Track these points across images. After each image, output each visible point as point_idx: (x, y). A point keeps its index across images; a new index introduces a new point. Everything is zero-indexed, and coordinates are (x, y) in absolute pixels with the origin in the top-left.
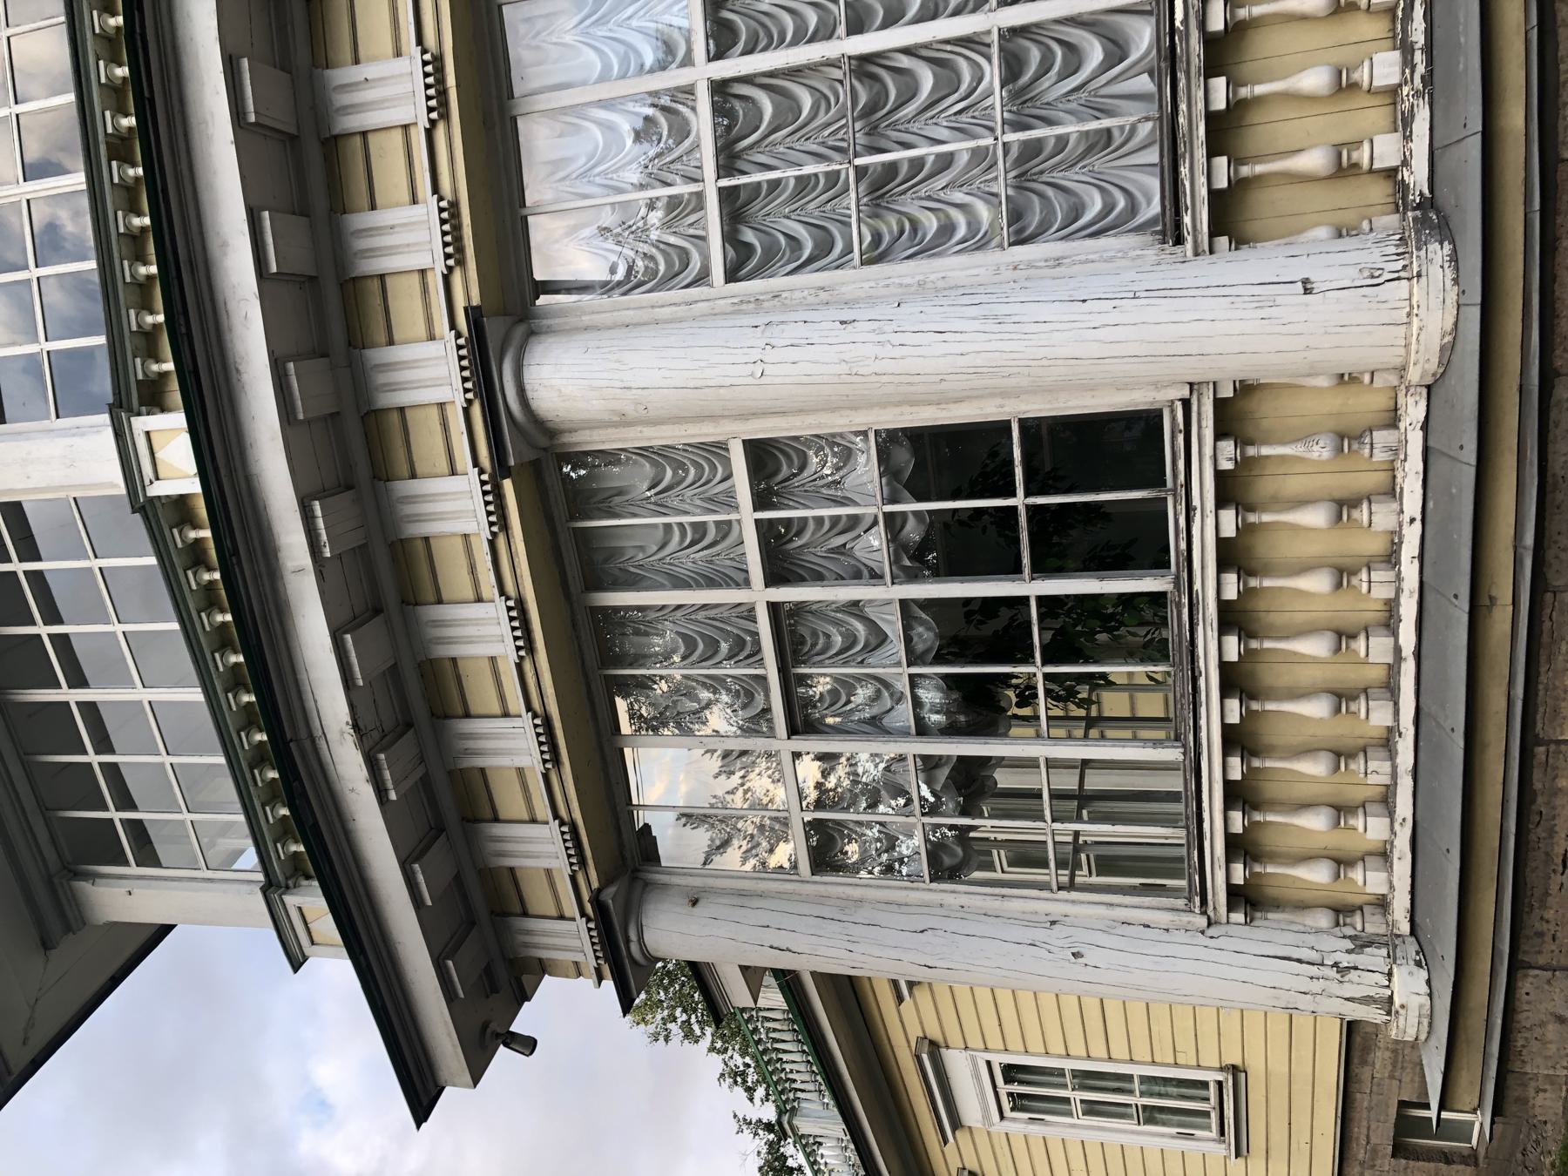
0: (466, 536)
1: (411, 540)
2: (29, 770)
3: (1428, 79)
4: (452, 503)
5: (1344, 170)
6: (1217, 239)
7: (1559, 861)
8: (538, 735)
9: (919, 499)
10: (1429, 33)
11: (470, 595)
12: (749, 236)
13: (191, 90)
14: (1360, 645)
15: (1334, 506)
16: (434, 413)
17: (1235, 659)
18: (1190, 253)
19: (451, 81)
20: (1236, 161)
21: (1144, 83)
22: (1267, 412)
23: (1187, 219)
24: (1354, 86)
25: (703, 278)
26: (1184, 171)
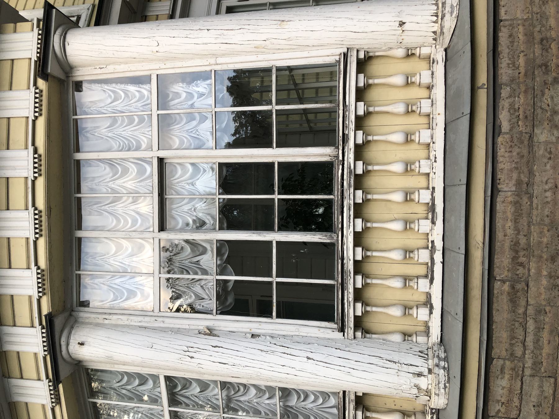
6: (357, 132)
8: (50, 390)
14: (414, 311)
15: (403, 309)
17: (360, 314)
20: (365, 220)
21: (335, 411)
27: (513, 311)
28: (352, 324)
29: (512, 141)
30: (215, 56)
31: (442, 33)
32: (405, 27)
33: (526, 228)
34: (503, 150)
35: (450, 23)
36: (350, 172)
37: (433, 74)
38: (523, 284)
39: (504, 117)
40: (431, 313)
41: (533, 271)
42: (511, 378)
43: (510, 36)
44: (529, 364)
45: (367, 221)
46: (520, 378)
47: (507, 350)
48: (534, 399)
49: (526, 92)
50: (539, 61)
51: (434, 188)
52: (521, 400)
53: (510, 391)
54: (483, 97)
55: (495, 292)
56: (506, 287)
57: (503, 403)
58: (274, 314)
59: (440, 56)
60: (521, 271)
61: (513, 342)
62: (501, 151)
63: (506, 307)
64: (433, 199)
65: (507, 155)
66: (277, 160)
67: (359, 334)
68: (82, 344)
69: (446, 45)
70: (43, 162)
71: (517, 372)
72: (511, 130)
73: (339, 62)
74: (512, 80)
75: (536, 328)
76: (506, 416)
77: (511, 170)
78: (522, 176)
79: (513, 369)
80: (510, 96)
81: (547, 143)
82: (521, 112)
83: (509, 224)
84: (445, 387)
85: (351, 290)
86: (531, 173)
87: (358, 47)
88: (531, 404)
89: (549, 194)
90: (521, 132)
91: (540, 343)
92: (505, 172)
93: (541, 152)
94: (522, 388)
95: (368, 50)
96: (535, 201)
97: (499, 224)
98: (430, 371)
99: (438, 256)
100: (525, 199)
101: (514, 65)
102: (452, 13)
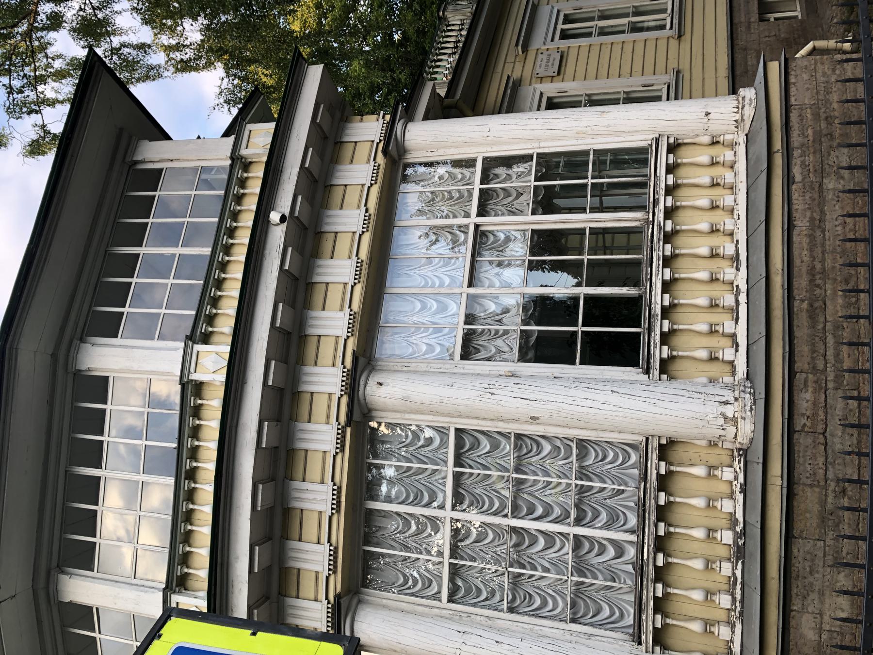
0: (317, 572)
1: (294, 509)
2: (65, 635)
3: (741, 613)
4: (321, 436)
5: (713, 359)
7: (810, 384)
9: (537, 325)
10: (742, 595)
11: (312, 596)
12: (460, 583)
13: (236, 494)
16: (316, 515)
18: (644, 651)
19: (343, 499)
21: (630, 568)
22: (677, 454)
23: (644, 637)
24: (717, 305)
25: (436, 597)
26: (644, 617)
27: (813, 326)
28: (657, 366)
29: (804, 188)
30: (539, 140)
31: (743, 120)
32: (710, 116)
33: (820, 255)
34: (796, 195)
35: (749, 112)
36: (660, 228)
37: (735, 153)
38: (821, 303)
39: (797, 171)
40: (737, 351)
41: (829, 292)
42: (815, 391)
43: (800, 115)
44: (831, 377)
45: (671, 464)
46: (823, 391)
47: (809, 364)
48: (839, 412)
49: (814, 153)
50: (824, 132)
51: (737, 241)
52: (826, 414)
53: (815, 403)
54: (778, 160)
55: (795, 309)
56: (805, 305)
57: (808, 417)
58: (578, 360)
59: (742, 139)
60: (818, 291)
61: (815, 355)
62: (795, 196)
63: (806, 324)
64: (737, 250)
65: (800, 198)
66: (588, 225)
67: (657, 649)
68: (381, 384)
69: (746, 132)
70: (371, 221)
71: (820, 385)
72: (803, 180)
73: (651, 145)
74: (803, 145)
75: (835, 342)
76: (811, 430)
77: (805, 210)
78: (815, 214)
79: (816, 382)
80: (801, 156)
81: (834, 189)
82: (811, 167)
83: (805, 252)
84: (751, 409)
85: (658, 332)
86: (822, 212)
87: (668, 133)
88: (837, 418)
89: (839, 228)
90: (812, 182)
91: (841, 357)
92: (799, 211)
93: (830, 197)
94: (826, 401)
95: (678, 137)
96: (827, 234)
97: (796, 252)
98: (736, 400)
99: (743, 298)
100: (818, 233)
101: (803, 134)
102: (750, 105)
